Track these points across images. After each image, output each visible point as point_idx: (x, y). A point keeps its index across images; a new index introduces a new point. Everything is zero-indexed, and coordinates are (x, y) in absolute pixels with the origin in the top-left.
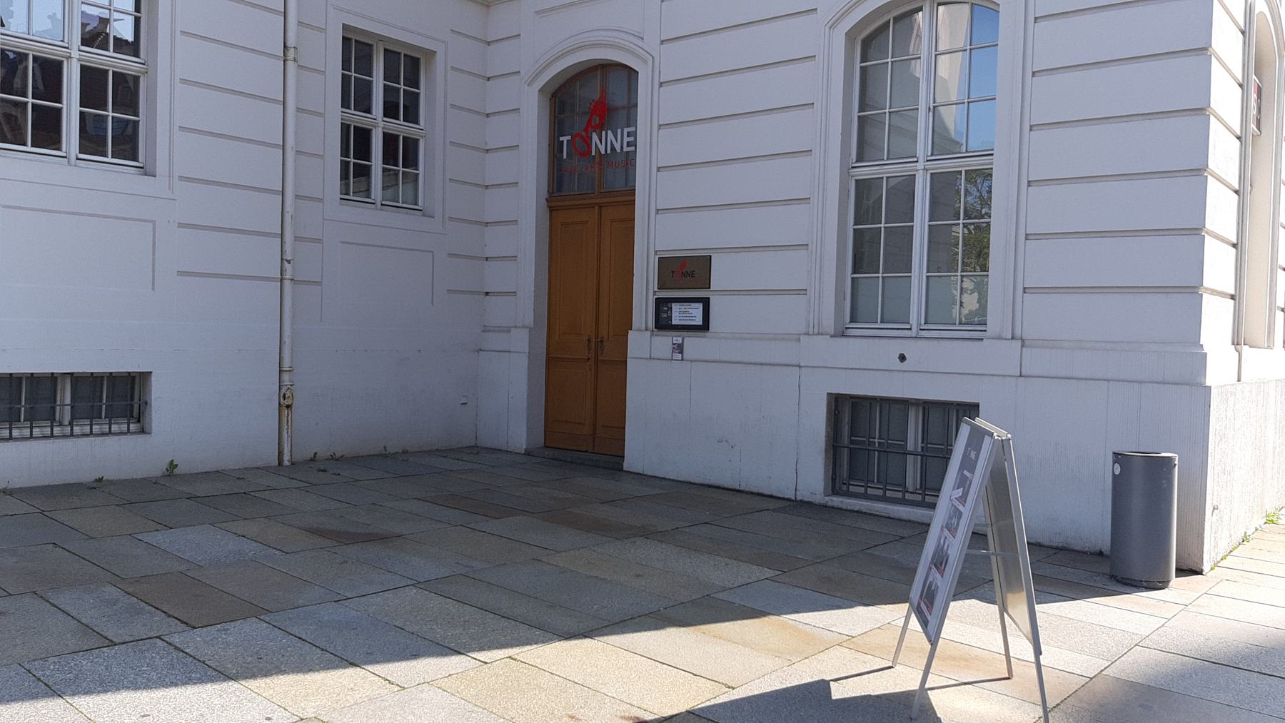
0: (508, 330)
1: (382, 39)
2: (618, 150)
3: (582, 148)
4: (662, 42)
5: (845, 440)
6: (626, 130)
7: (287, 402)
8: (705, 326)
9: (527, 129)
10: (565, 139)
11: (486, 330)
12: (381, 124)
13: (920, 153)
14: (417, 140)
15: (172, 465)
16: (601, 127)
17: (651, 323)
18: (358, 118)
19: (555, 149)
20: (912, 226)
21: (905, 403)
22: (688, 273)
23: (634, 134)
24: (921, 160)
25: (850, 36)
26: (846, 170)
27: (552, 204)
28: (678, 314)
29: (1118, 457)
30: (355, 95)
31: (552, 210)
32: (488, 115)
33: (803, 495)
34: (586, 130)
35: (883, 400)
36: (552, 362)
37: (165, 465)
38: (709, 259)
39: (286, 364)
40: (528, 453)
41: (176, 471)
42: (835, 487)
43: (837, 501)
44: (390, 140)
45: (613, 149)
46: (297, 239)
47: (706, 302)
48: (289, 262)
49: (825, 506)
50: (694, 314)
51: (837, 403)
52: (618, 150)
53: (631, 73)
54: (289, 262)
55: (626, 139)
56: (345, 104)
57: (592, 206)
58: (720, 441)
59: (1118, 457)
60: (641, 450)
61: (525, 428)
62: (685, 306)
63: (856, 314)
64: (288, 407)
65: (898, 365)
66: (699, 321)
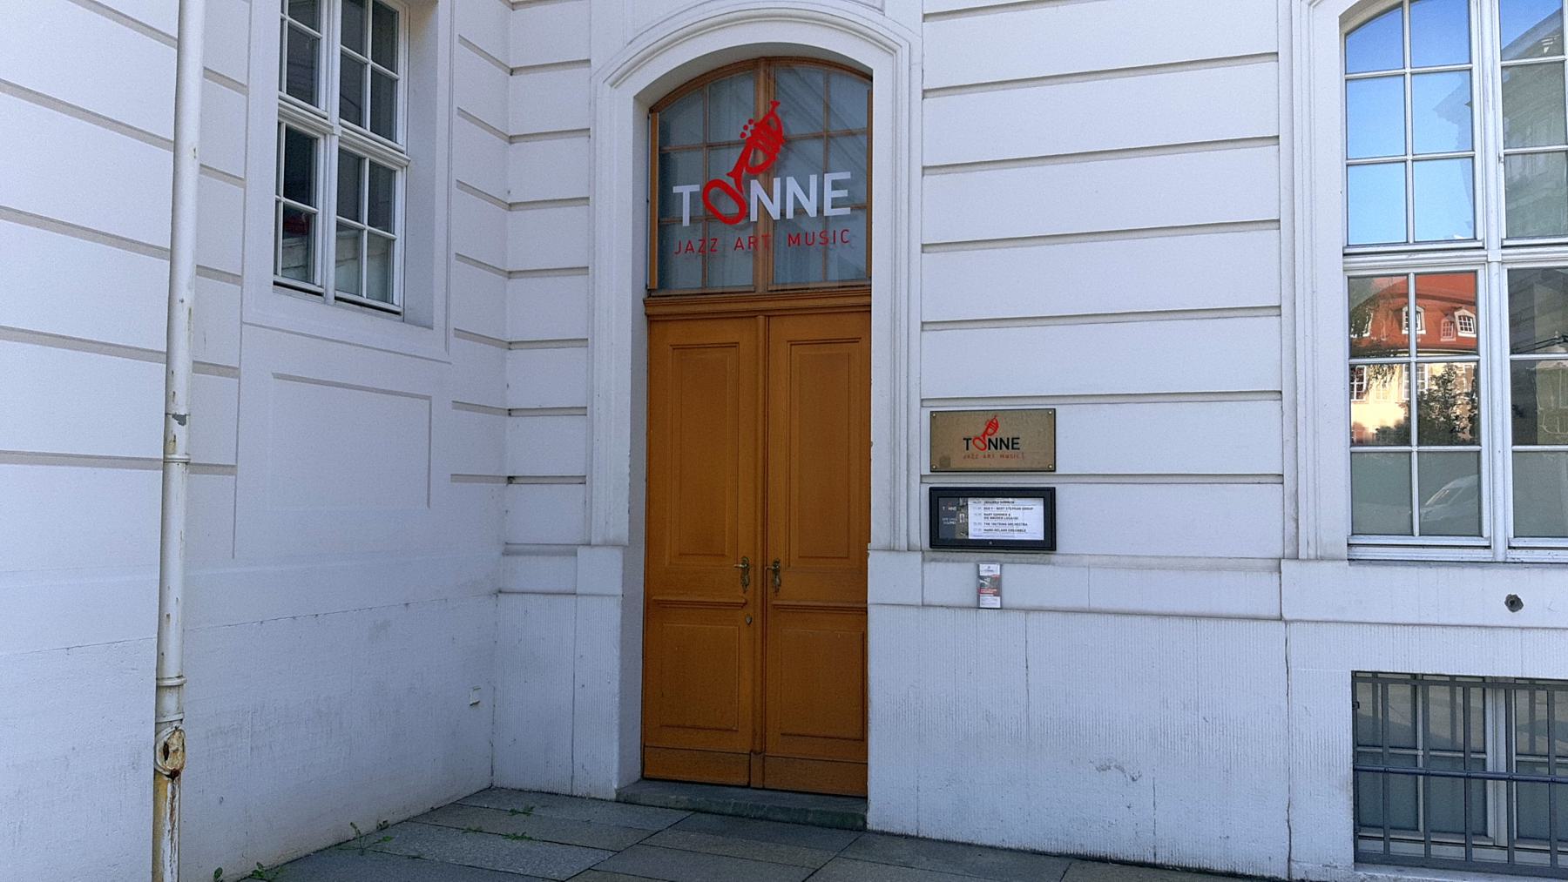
0: (570, 551)
2: (812, 212)
4: (925, 17)
6: (828, 178)
7: (170, 765)
8: (1048, 544)
11: (509, 550)
12: (338, 130)
14: (392, 172)
16: (766, 171)
22: (998, 449)
24: (1494, 244)
25: (1344, 19)
27: (652, 311)
31: (652, 320)
32: (511, 139)
34: (735, 174)
38: (1053, 414)
39: (172, 670)
40: (624, 799)
44: (350, 162)
45: (800, 211)
46: (199, 366)
47: (1048, 497)
48: (182, 420)
50: (1027, 520)
52: (812, 212)
53: (865, 76)
54: (182, 420)
55: (829, 194)
57: (752, 315)
58: (1103, 769)
61: (616, 749)
64: (174, 775)
65: (1505, 616)
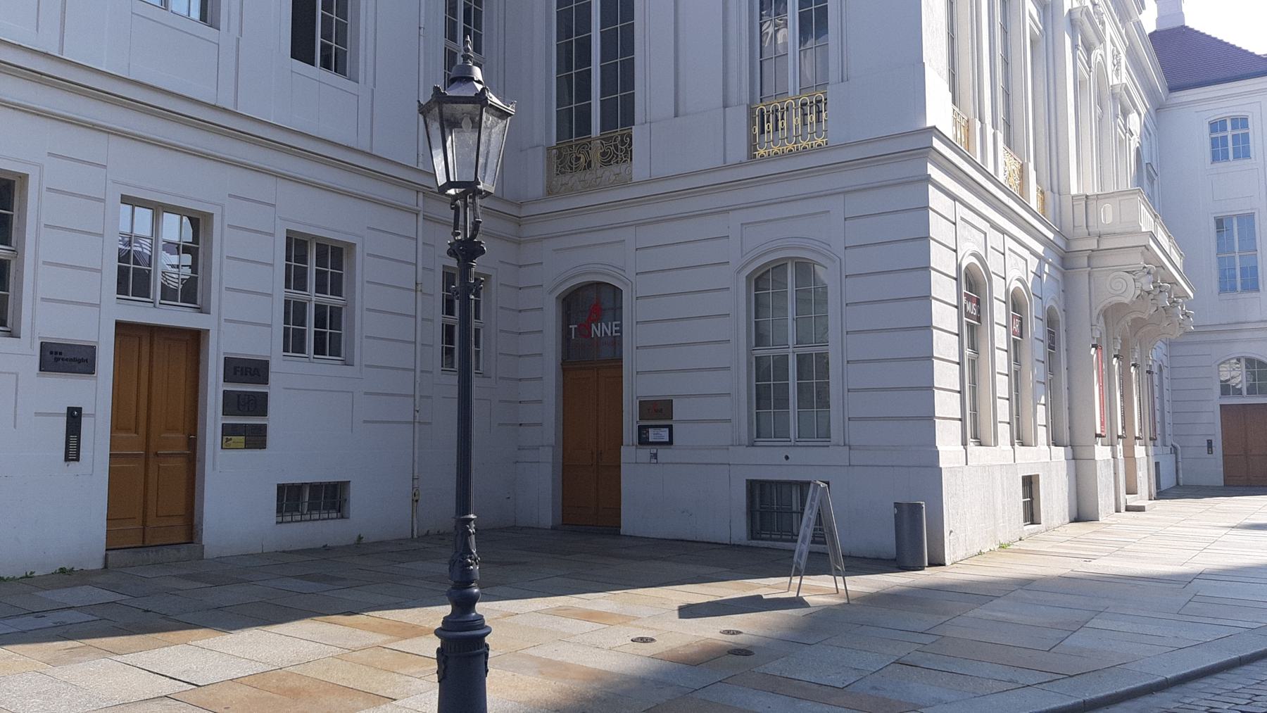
1: (314, 237)
3: (584, 330)
5: (758, 507)
8: (670, 442)
9: (549, 321)
10: (573, 327)
13: (790, 343)
15: (360, 538)
16: (597, 320)
17: (636, 440)
18: (297, 295)
19: (566, 333)
20: (788, 386)
21: (790, 483)
22: (657, 410)
23: (621, 326)
26: (750, 351)
28: (653, 435)
29: (897, 505)
30: (295, 279)
31: (564, 370)
33: (735, 541)
35: (772, 482)
36: (565, 468)
37: (356, 538)
40: (553, 528)
41: (364, 541)
42: (753, 534)
43: (754, 543)
47: (670, 428)
49: (747, 547)
51: (752, 485)
53: (617, 292)
56: (287, 286)
59: (897, 505)
60: (632, 521)
62: (657, 430)
63: (759, 433)
66: (667, 439)
